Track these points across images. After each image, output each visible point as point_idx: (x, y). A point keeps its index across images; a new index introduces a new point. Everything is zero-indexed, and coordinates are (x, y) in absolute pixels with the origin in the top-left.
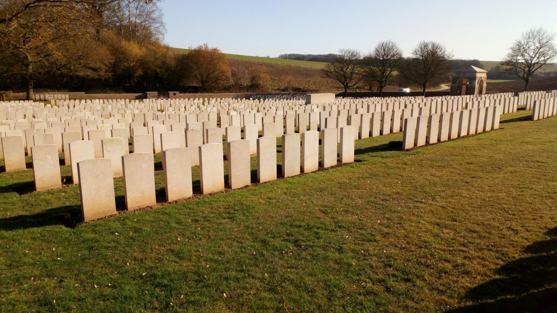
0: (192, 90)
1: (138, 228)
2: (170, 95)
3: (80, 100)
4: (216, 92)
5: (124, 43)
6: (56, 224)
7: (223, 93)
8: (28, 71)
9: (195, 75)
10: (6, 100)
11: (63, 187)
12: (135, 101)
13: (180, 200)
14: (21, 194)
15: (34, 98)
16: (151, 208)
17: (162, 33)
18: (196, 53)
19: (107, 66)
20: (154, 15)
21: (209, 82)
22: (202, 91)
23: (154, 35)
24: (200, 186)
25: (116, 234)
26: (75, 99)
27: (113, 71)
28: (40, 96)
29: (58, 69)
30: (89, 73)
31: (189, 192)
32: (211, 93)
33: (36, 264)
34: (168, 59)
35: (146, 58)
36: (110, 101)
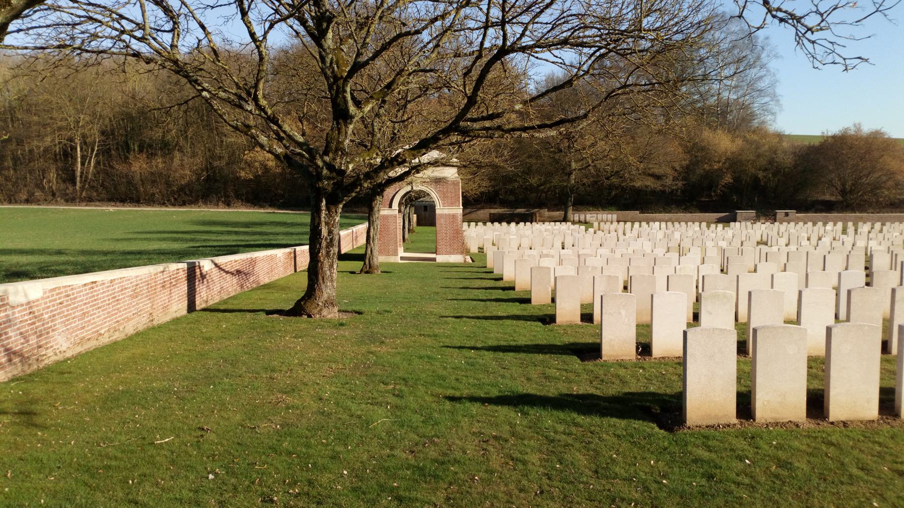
0: (820, 207)
1: (784, 460)
2: (778, 216)
3: (633, 223)
4: (872, 210)
5: (707, 134)
6: (644, 420)
7: (887, 212)
8: (568, 180)
9: (830, 181)
10: (539, 221)
11: (637, 359)
12: (716, 227)
13: (852, 422)
14: (582, 360)
15: (572, 219)
16: (797, 426)
17: (773, 111)
18: (835, 141)
19: (676, 170)
20: (761, 85)
21: (859, 192)
22: (842, 208)
23: (759, 116)
24: (893, 400)
25: (747, 461)
26: (625, 222)
27: (684, 179)
28: (585, 217)
29: (608, 178)
30: (650, 183)
31: (872, 410)
32: (861, 212)
33: (632, 480)
34: (781, 155)
35: (741, 155)
36: (676, 224)
